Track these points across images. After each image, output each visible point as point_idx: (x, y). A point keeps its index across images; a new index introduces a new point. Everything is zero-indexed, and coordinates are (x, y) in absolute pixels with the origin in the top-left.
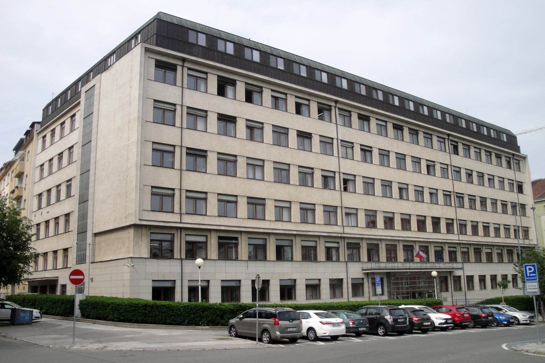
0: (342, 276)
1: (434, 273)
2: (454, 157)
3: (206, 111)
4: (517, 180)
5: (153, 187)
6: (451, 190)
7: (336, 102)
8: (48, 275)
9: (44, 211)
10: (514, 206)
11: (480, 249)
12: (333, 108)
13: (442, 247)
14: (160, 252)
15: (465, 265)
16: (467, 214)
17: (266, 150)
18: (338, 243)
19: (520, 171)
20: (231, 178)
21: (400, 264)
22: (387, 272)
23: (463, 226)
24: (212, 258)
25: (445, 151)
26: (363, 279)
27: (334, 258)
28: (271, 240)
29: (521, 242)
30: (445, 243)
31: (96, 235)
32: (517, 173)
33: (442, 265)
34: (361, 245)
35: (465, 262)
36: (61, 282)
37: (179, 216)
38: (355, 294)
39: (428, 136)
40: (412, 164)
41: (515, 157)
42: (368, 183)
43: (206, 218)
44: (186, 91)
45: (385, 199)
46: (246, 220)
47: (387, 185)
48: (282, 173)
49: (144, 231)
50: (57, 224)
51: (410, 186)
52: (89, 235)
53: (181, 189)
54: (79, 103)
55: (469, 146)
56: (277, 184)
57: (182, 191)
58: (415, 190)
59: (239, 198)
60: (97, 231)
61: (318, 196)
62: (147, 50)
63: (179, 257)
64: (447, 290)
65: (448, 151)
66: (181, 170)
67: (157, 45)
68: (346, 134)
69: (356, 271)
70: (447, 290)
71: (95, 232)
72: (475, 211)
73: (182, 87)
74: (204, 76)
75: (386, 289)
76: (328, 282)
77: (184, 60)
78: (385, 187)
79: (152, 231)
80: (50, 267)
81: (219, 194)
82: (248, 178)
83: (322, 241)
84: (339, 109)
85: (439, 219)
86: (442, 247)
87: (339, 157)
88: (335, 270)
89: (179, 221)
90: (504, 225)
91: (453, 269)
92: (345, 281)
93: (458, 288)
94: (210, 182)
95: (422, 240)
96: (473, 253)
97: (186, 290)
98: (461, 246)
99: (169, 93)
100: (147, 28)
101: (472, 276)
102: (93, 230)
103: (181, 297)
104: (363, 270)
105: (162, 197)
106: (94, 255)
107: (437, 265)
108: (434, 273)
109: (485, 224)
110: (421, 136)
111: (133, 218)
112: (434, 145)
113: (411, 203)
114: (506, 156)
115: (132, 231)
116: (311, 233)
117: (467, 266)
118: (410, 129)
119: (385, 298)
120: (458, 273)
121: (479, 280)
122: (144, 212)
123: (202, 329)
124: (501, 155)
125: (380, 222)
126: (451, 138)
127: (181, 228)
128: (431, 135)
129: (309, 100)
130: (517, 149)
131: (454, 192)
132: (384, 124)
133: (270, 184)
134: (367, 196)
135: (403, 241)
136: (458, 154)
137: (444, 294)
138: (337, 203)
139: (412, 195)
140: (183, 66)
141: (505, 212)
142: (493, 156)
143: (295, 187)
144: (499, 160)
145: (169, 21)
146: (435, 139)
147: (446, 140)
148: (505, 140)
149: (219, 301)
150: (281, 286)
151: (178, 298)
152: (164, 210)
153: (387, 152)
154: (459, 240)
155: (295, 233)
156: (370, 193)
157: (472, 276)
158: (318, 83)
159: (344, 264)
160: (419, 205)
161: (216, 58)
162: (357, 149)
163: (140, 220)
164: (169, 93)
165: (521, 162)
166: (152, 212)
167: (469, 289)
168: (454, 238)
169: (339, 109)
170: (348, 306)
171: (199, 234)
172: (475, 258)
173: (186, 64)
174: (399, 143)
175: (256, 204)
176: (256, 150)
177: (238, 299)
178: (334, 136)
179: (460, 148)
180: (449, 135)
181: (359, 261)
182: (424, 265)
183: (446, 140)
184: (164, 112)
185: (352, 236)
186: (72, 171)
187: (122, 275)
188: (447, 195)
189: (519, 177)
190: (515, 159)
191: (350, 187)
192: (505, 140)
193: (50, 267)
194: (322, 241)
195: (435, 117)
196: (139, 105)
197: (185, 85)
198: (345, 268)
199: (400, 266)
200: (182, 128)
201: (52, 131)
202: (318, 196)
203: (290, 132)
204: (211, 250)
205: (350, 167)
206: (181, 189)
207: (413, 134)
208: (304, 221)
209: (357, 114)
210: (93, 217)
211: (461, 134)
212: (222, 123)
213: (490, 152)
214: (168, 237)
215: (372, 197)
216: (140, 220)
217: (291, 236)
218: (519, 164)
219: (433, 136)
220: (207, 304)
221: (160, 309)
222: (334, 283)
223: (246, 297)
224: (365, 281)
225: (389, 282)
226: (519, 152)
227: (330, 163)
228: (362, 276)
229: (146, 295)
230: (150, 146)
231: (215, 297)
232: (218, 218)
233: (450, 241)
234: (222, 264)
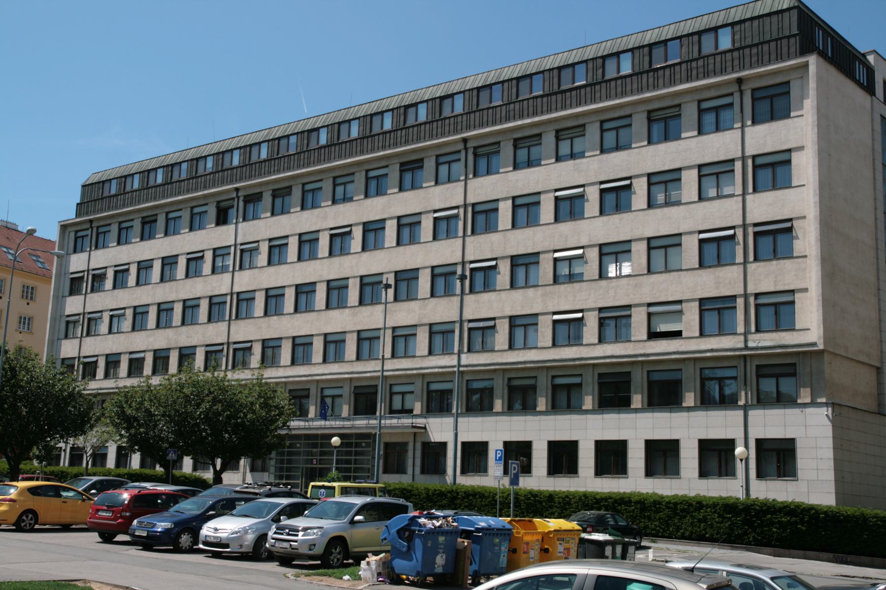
120: (436, 436)
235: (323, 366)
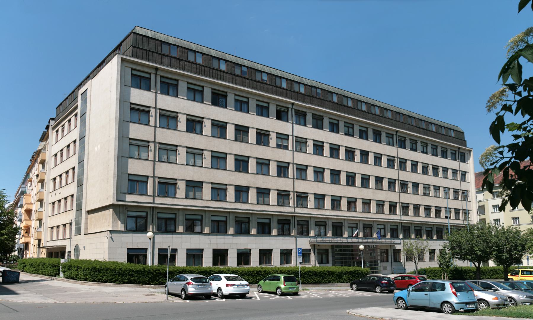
1: (362, 247)
2: (401, 150)
4: (399, 156)
8: (59, 243)
9: (57, 192)
10: (456, 191)
12: (290, 110)
13: (432, 228)
23: (405, 208)
26: (310, 250)
28: (231, 217)
29: (460, 222)
31: (89, 212)
33: (370, 240)
34: (251, 219)
36: (68, 249)
37: (152, 198)
43: (176, 199)
44: (295, 125)
47: (379, 180)
48: (242, 164)
50: (66, 203)
56: (260, 176)
60: (88, 209)
61: (273, 182)
62: (123, 60)
66: (154, 161)
67: (132, 56)
69: (304, 243)
75: (330, 258)
80: (61, 237)
82: (187, 165)
88: (288, 243)
91: (394, 243)
92: (150, 251)
94: (251, 179)
99: (140, 96)
101: (270, 251)
107: (365, 241)
108: (362, 247)
111: (112, 199)
117: (431, 242)
120: (398, 247)
121: (281, 253)
122: (121, 194)
123: (149, 287)
130: (464, 143)
135: (277, 215)
137: (384, 264)
138: (397, 200)
141: (447, 197)
149: (211, 265)
150: (128, 254)
151: (149, 262)
153: (225, 124)
155: (251, 212)
156: (265, 172)
157: (270, 251)
160: (365, 190)
161: (186, 67)
170: (289, 271)
176: (263, 152)
177: (201, 263)
182: (355, 240)
184: (139, 113)
186: (73, 162)
187: (99, 245)
188: (392, 183)
192: (528, 158)
193: (61, 237)
196: (116, 107)
199: (344, 240)
201: (62, 126)
202: (273, 182)
203: (229, 126)
205: (301, 158)
208: (349, 209)
215: (321, 183)
221: (133, 271)
224: (312, 252)
228: (309, 247)
234: (281, 239)
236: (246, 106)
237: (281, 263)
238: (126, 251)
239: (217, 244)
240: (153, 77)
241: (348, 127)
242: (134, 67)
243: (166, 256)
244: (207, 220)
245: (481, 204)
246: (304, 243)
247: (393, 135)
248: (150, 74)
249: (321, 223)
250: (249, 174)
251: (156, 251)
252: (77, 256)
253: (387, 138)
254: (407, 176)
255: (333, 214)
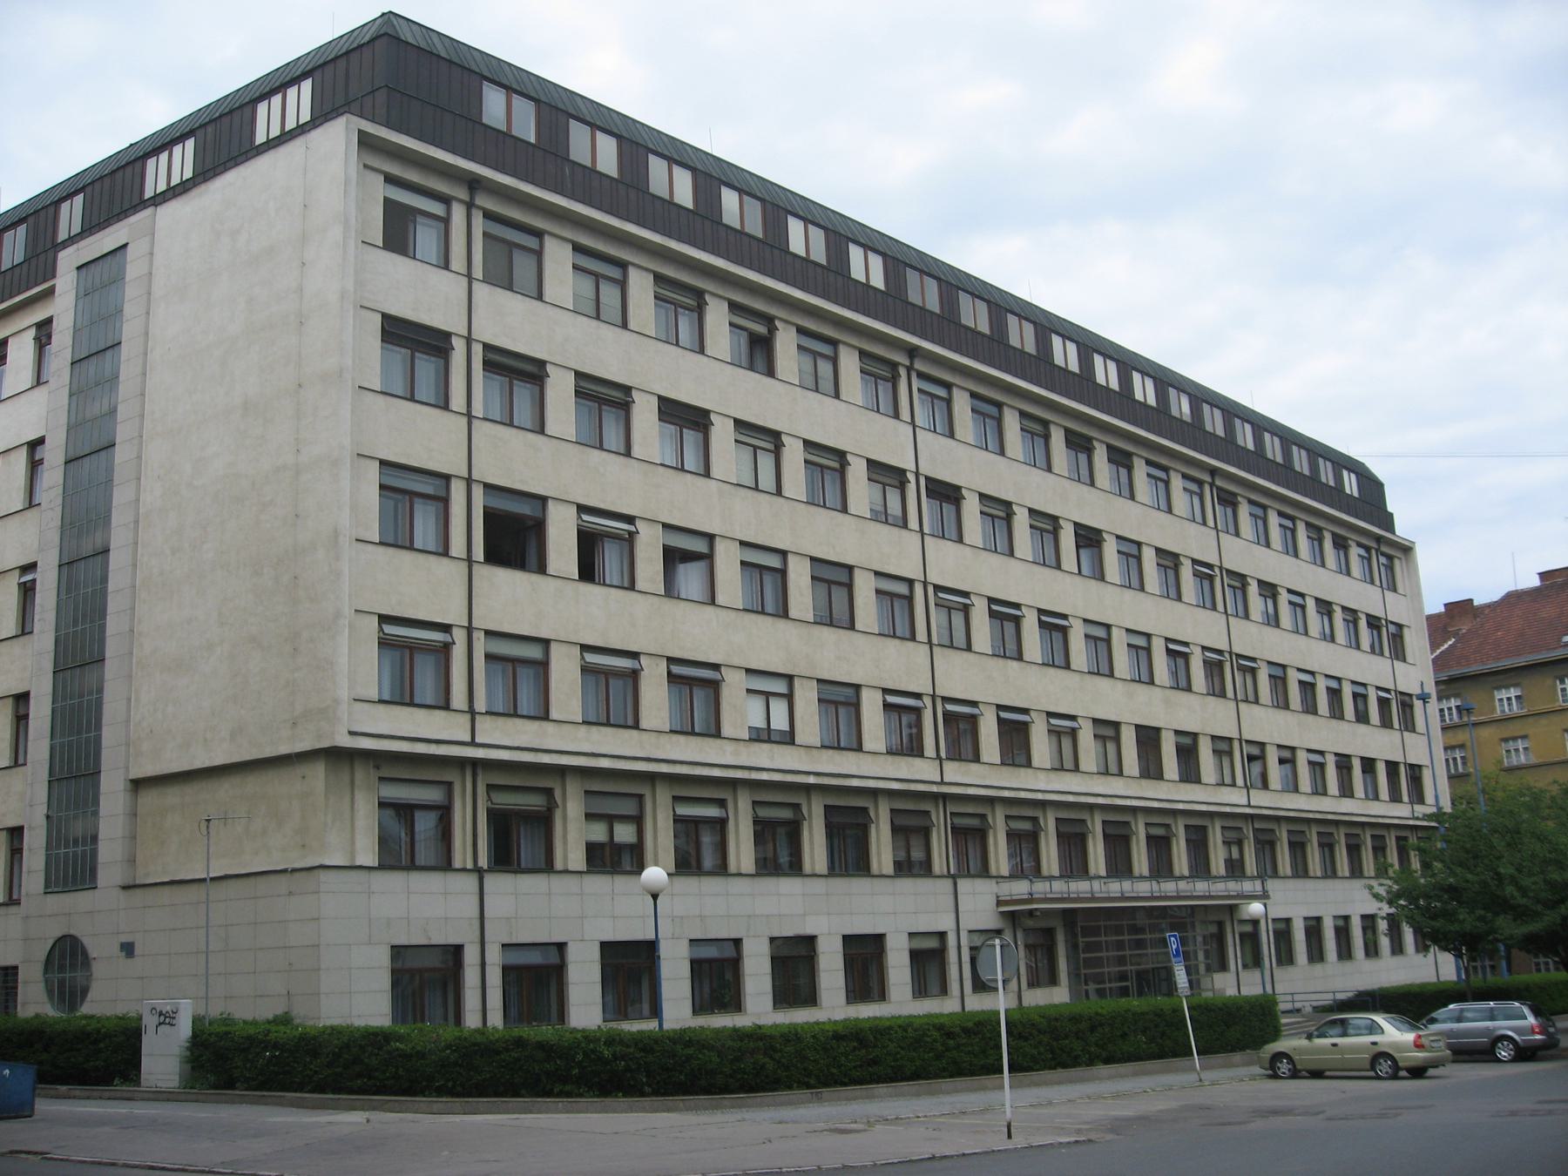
0: (945, 923)
3: (627, 390)
5: (384, 619)
6: (1223, 646)
7: (913, 352)
11: (1127, 824)
12: (903, 372)
13: (1035, 820)
14: (409, 842)
15: (1271, 884)
16: (1268, 725)
17: (724, 506)
18: (722, 803)
19: (1395, 590)
20: (841, 631)
21: (1098, 887)
22: (1065, 911)
23: (961, 728)
24: (571, 868)
25: (1204, 523)
27: (708, 861)
28: (740, 804)
30: (991, 801)
31: (138, 785)
32: (1389, 595)
34: (805, 811)
35: (969, 875)
38: (921, 989)
39: (1160, 473)
40: (983, 523)
41: (1384, 549)
42: (762, 568)
44: (482, 291)
45: (1052, 671)
46: (667, 737)
47: (834, 578)
49: (361, 773)
51: (720, 547)
52: (112, 786)
53: (470, 630)
54: (51, 292)
55: (1045, 424)
57: (475, 635)
58: (878, 592)
59: (643, 660)
62: (366, 142)
63: (470, 865)
64: (1223, 967)
65: (1211, 523)
66: (469, 560)
68: (508, 321)
70: (1223, 967)
71: (139, 772)
72: (1288, 713)
73: (469, 276)
74: (531, 242)
76: (765, 949)
77: (474, 184)
78: (823, 588)
79: (386, 773)
81: (585, 648)
83: (663, 796)
84: (488, 215)
85: (1373, 760)
86: (797, 807)
87: (923, 534)
89: (468, 738)
90: (1000, 707)
92: (471, 957)
93: (1255, 961)
95: (1156, 805)
96: (1183, 843)
97: (495, 978)
98: (951, 808)
100: (342, 63)
101: (878, 940)
102: (127, 768)
103: (483, 1006)
104: (999, 903)
105: (412, 655)
106: (132, 861)
109: (891, 699)
110: (1140, 470)
112: (708, 342)
113: (1119, 684)
114: (1185, 476)
115: (318, 773)
116: (855, 783)
118: (1110, 447)
119: (1059, 995)
124: (1235, 495)
125: (1041, 746)
126: (918, 365)
127: (475, 764)
128: (834, 343)
129: (948, 386)
130: (1387, 521)
131: (1230, 653)
132: (942, 392)
133: (733, 614)
134: (1001, 661)
136: (770, 372)
139: (867, 607)
140: (470, 206)
142: (1057, 438)
143: (804, 629)
144: (1083, 457)
145: (423, 45)
146: (849, 363)
147: (1207, 488)
148: (1356, 494)
152: (417, 700)
154: (1249, 806)
155: (812, 780)
158: (819, 270)
159: (470, 882)
162: (794, 455)
163: (351, 733)
164: (428, 294)
165: (1397, 562)
166: (381, 707)
167: (1280, 962)
168: (919, 772)
169: (921, 375)
171: (516, 783)
172: (1011, 856)
173: (483, 201)
174: (1037, 475)
175: (697, 684)
178: (910, 466)
179: (786, 343)
180: (1214, 472)
181: (984, 872)
182: (1219, 888)
183: (1207, 488)
185: (971, 791)
188: (898, 596)
189: (1395, 608)
190: (1383, 554)
191: (610, 559)
192: (1356, 494)
194: (663, 796)
195: (1240, 442)
197: (478, 272)
198: (952, 897)
200: (469, 415)
204: (565, 843)
205: (951, 564)
206: (470, 630)
207: (876, 377)
209: (1063, 432)
210: (128, 721)
211: (1249, 471)
212: (400, 354)
213: (1045, 424)
214: (433, 795)
215: (1015, 664)
216: (351, 733)
217: (724, 787)
218: (1390, 568)
219: (842, 350)
220: (544, 1032)
222: (785, 952)
223: (585, 1007)
225: (1073, 947)
226: (1393, 532)
227: (898, 552)
229: (365, 1003)
230: (373, 473)
231: (483, 1006)
232: (584, 728)
233: (1228, 809)
235: (1053, 775)
236: (531, 262)
237: (698, 1009)
238: (384, 958)
239: (702, 917)
240: (458, 213)
241: (816, 355)
242: (739, 298)
243: (536, 977)
244: (660, 817)
245: (125, 939)
246: (979, 903)
247: (894, 366)
248: (446, 200)
249: (1026, 820)
250: (790, 623)
251: (494, 957)
252: (69, 993)
253: (807, 361)
254: (966, 565)
255: (1042, 786)
